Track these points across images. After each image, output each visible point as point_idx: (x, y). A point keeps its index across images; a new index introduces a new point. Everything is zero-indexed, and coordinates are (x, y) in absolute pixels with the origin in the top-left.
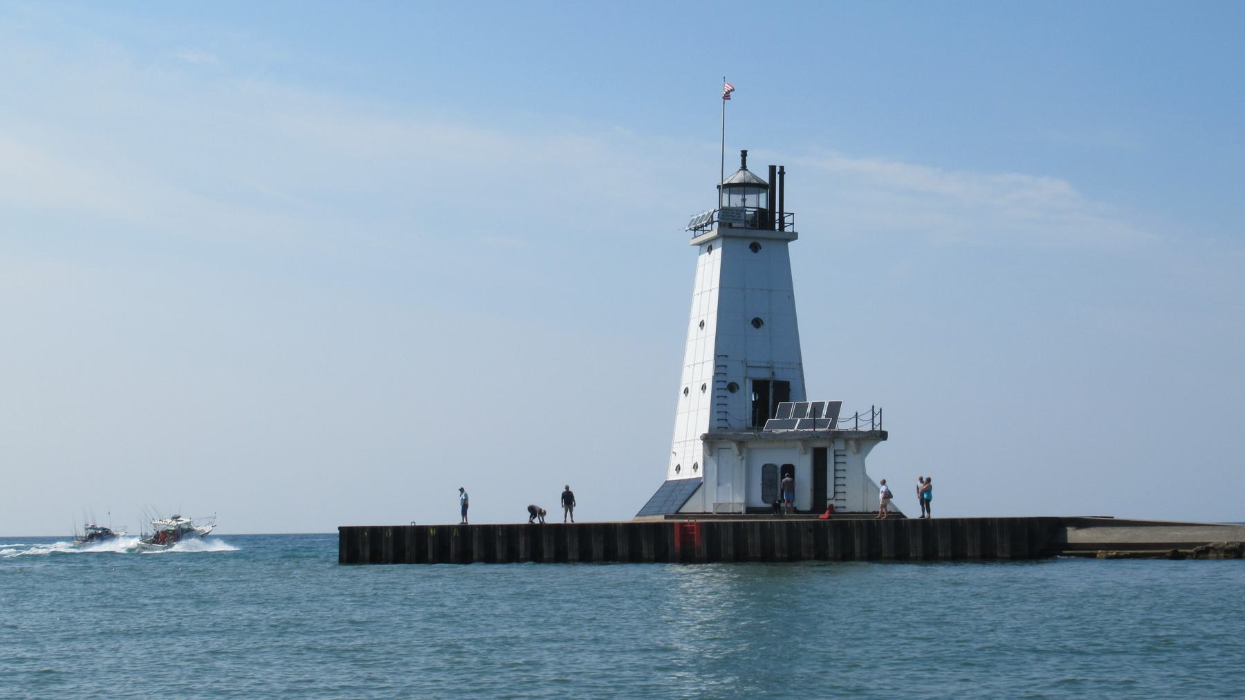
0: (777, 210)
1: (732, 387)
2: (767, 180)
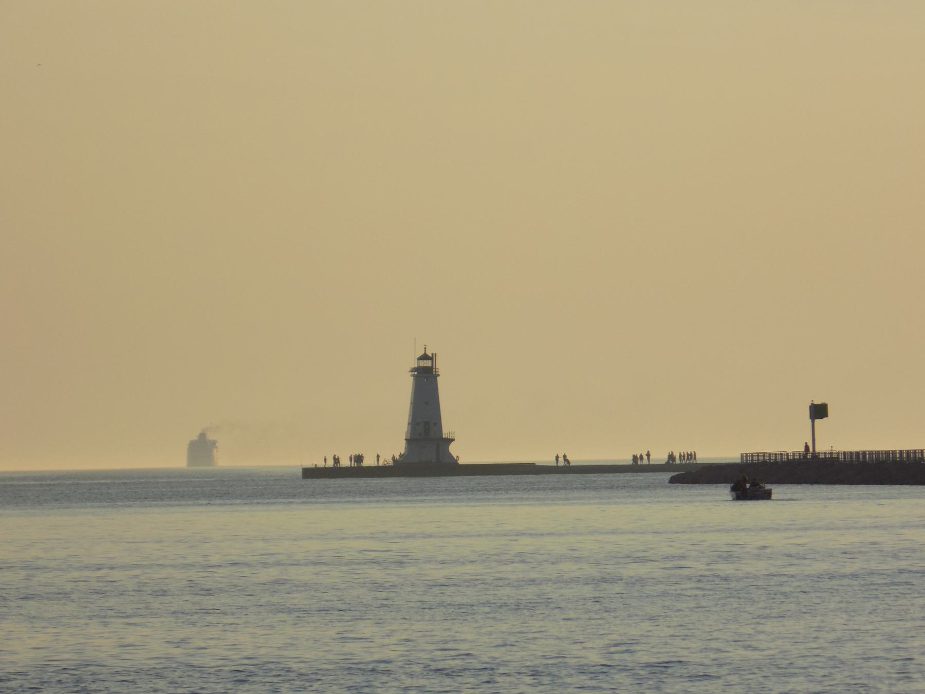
0: (434, 367)
1: (418, 424)
2: (431, 356)
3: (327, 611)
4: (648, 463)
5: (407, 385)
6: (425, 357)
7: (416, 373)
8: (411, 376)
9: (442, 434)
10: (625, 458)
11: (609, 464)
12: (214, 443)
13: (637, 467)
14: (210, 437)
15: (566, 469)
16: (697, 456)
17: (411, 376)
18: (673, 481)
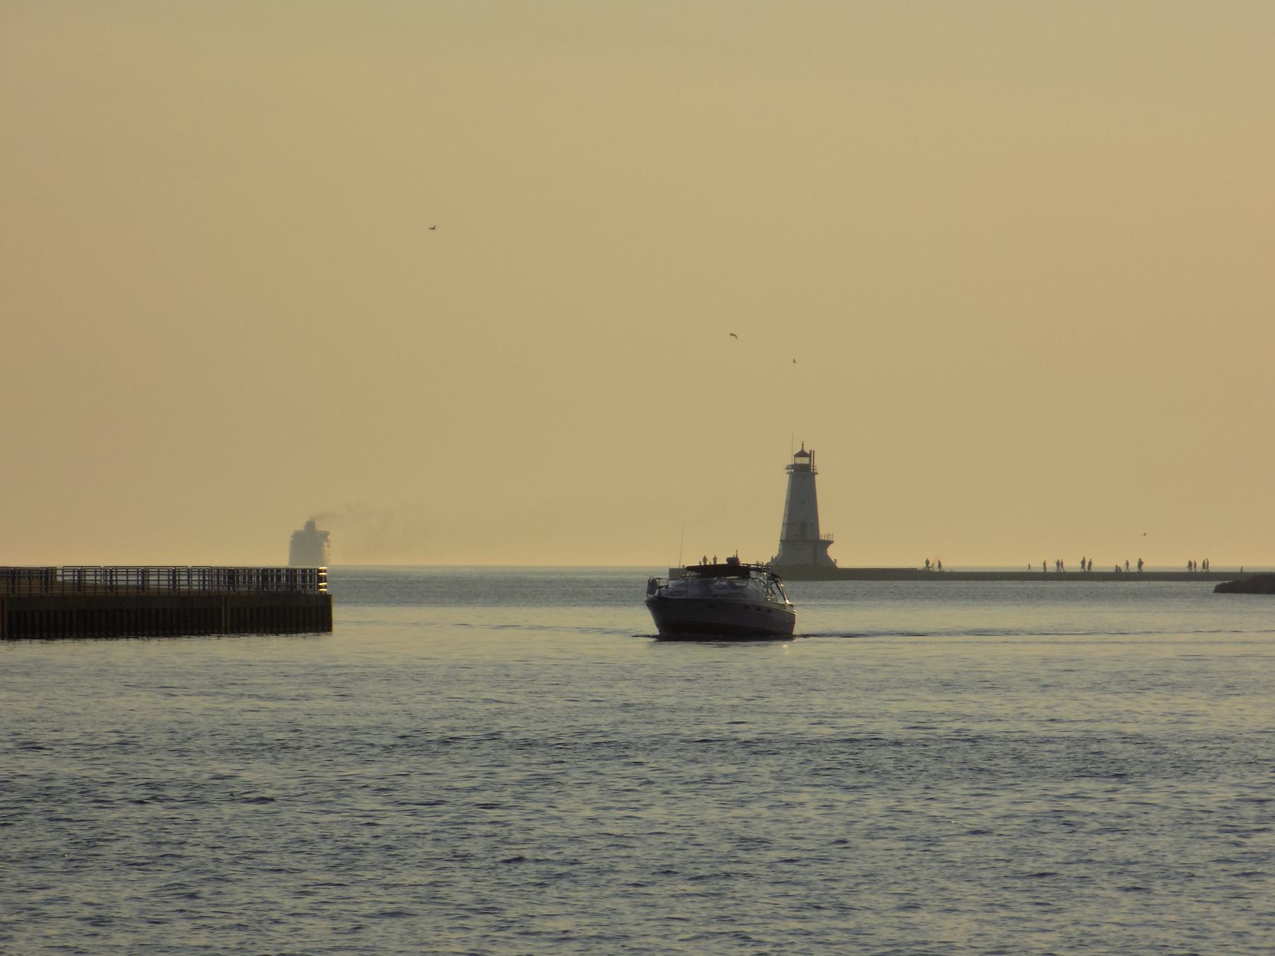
2: (809, 452)
3: (413, 746)
4: (1043, 570)
5: (780, 486)
6: (802, 454)
7: (793, 471)
8: (787, 473)
9: (819, 536)
10: (1180, 565)
11: (1167, 571)
12: (326, 534)
13: (1190, 576)
14: (320, 527)
15: (1087, 575)
16: (1064, 565)
17: (787, 473)
18: (1219, 590)
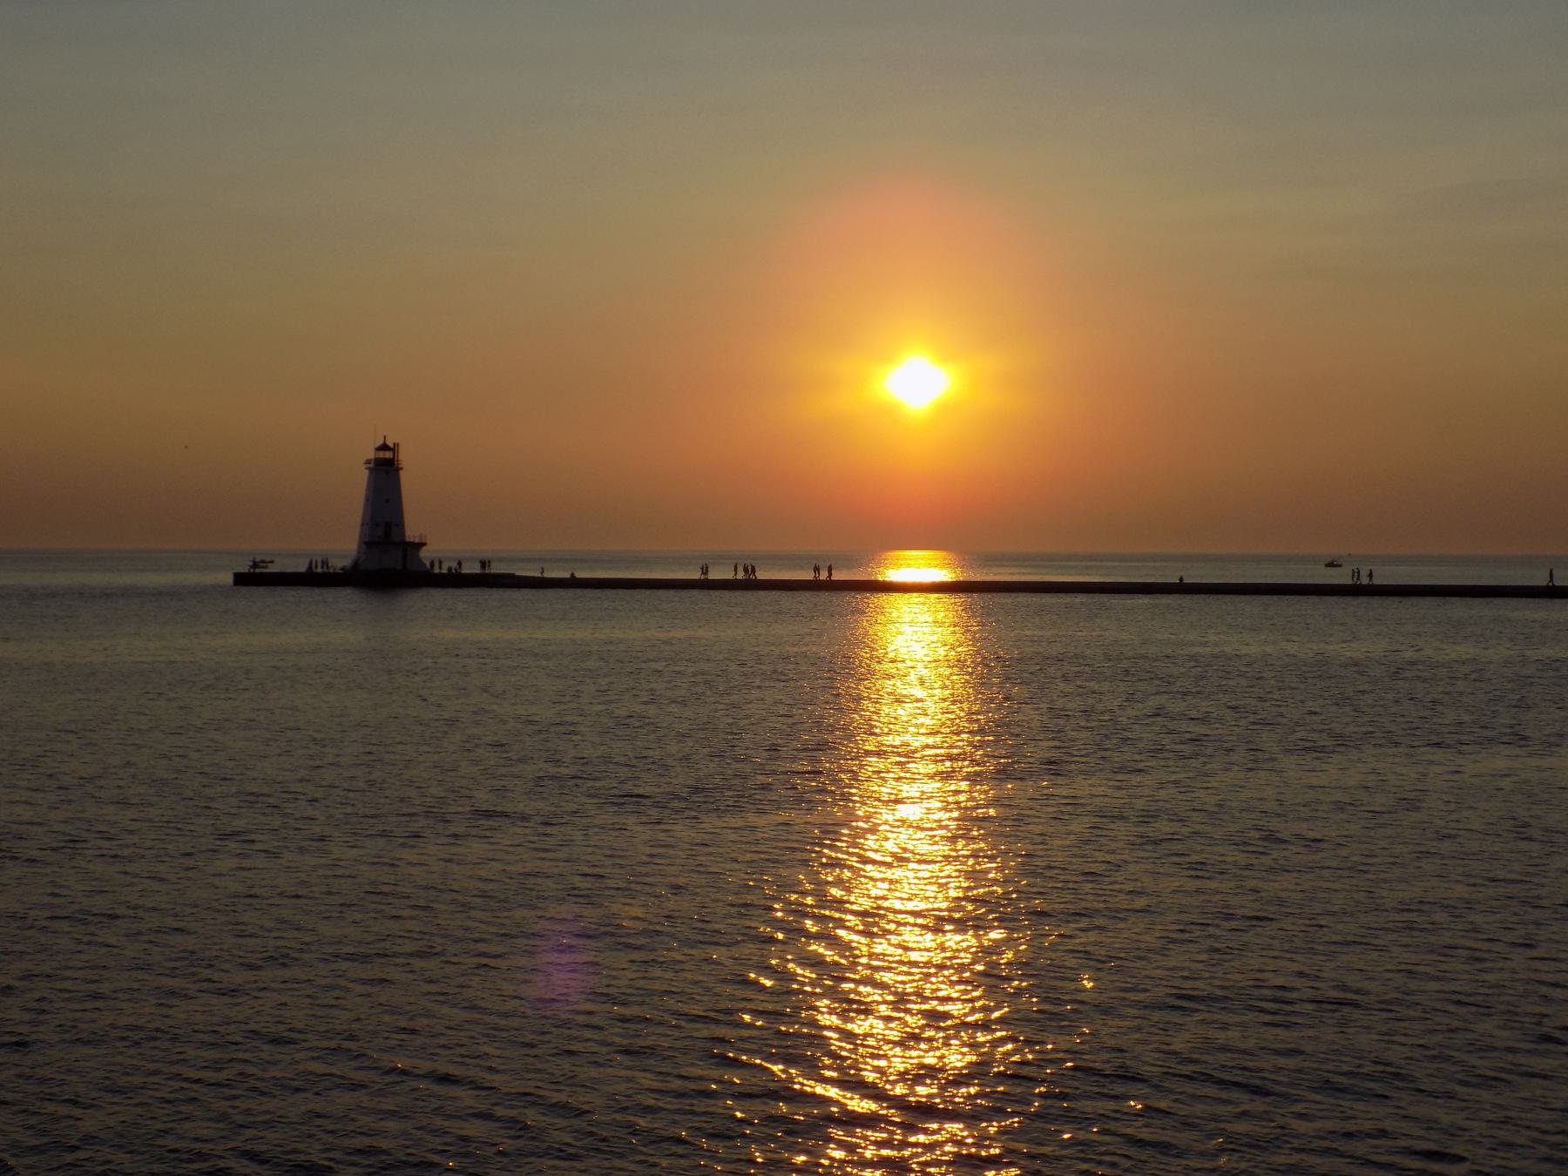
1: (377, 525)
2: (392, 446)
6: (384, 447)
